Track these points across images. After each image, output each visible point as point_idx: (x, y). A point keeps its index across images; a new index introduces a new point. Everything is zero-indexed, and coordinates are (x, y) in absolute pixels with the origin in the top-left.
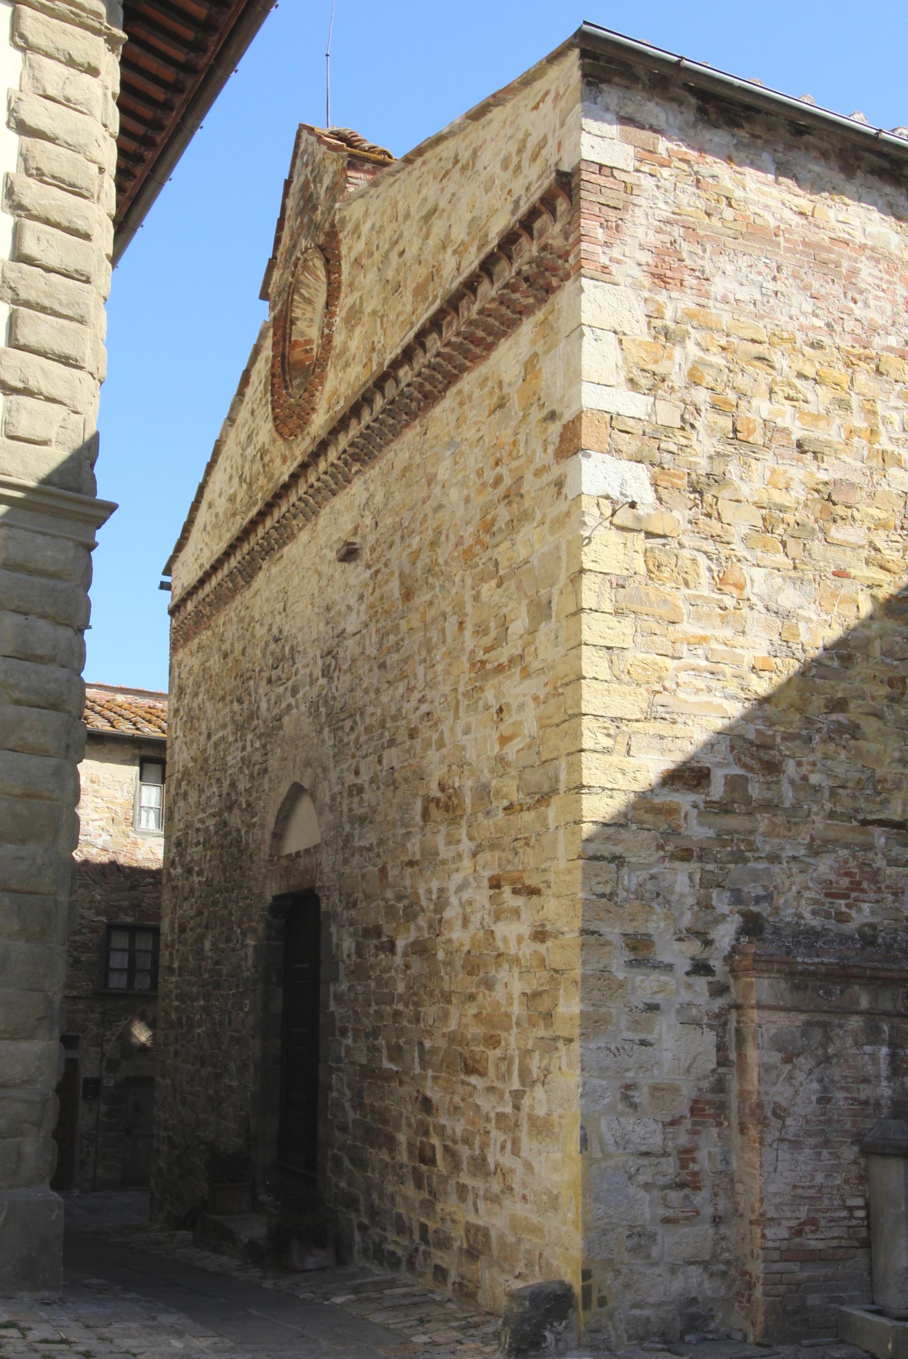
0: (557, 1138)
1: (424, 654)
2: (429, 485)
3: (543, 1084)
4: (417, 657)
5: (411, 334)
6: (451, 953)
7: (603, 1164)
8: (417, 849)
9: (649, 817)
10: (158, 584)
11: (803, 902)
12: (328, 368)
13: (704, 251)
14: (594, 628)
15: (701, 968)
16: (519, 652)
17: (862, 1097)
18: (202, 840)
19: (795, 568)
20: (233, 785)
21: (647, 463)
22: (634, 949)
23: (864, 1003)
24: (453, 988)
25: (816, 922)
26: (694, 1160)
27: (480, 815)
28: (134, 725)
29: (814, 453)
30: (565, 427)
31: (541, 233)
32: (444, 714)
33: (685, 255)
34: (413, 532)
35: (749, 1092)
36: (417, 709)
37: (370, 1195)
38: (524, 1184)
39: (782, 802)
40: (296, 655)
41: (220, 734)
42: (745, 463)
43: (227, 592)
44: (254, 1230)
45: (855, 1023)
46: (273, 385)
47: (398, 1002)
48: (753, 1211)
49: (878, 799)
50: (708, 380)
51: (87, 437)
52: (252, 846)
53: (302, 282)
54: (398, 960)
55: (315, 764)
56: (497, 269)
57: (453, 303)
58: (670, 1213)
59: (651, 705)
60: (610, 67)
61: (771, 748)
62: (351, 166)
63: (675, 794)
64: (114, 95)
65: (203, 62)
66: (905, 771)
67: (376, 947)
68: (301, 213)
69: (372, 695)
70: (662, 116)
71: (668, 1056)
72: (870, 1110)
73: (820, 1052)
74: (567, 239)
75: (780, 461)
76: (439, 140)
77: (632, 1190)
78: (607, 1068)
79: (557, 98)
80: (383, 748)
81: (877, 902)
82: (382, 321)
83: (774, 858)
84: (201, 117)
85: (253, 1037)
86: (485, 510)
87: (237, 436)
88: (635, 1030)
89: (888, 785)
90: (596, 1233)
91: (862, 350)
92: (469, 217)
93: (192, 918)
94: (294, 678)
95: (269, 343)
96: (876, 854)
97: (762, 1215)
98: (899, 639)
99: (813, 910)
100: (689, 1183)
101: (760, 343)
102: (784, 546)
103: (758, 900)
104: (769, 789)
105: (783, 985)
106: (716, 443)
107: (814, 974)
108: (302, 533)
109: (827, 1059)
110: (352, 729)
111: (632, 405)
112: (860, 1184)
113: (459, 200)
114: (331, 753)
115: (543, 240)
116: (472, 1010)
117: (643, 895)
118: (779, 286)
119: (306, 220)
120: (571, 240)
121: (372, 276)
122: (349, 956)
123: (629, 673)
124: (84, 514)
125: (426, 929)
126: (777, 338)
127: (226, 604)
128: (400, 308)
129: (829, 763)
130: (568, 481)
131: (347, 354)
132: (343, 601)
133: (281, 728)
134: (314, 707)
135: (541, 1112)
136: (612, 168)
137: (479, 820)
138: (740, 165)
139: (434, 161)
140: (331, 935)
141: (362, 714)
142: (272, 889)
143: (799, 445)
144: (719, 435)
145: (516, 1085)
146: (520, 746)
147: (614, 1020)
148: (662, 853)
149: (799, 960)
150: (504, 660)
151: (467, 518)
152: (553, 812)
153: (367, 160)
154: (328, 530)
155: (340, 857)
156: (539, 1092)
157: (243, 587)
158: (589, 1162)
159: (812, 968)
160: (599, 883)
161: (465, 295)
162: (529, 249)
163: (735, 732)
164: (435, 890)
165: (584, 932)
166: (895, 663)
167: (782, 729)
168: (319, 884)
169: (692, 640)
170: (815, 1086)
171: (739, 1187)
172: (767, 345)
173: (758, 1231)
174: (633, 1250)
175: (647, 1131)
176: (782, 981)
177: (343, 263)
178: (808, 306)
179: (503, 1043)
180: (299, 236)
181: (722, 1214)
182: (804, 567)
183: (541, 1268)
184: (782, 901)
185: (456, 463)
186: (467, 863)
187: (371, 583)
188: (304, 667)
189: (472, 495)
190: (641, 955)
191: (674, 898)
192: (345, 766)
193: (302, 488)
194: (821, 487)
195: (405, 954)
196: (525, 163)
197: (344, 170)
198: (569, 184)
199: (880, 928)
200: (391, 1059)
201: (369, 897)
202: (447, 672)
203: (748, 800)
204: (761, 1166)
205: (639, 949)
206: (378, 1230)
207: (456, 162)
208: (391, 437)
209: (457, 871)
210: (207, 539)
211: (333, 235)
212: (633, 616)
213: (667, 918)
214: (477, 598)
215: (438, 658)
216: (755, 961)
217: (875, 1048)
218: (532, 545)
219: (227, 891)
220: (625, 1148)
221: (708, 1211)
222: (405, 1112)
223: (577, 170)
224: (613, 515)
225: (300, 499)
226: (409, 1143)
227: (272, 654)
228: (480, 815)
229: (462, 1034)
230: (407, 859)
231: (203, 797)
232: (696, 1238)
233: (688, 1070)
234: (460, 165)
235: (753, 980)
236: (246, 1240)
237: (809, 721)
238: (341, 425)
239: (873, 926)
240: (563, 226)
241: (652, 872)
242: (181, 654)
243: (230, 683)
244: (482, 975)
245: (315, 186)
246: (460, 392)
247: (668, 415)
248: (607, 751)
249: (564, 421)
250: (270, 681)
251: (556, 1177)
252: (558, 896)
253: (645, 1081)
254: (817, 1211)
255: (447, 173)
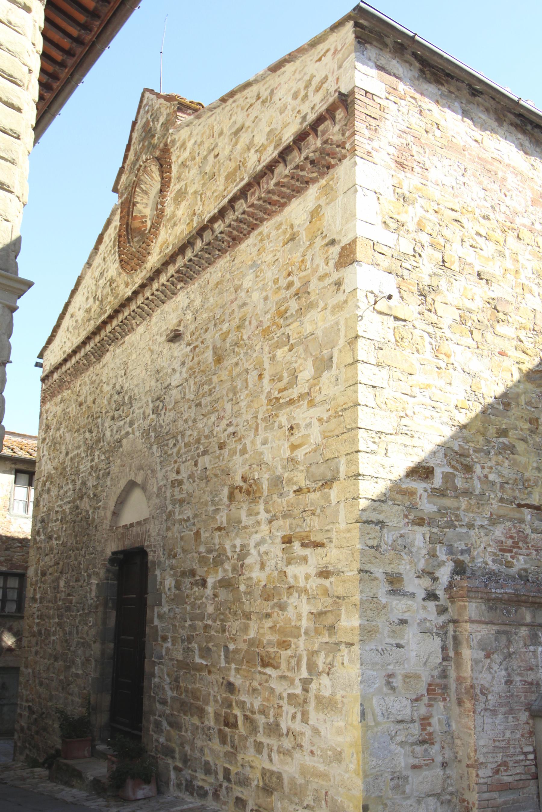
0: (341, 712)
1: (231, 395)
2: (236, 292)
3: (328, 674)
4: (225, 398)
5: (226, 200)
6: (251, 586)
7: (375, 730)
8: (224, 519)
9: (399, 497)
10: (34, 363)
11: (487, 554)
12: (161, 228)
13: (425, 152)
14: (364, 373)
15: (431, 596)
16: (307, 390)
17: (530, 680)
18: (60, 518)
19: (478, 348)
20: (84, 483)
21: (395, 274)
22: (391, 583)
23: (528, 619)
24: (251, 610)
25: (494, 567)
26: (430, 724)
27: (275, 497)
28: (12, 450)
29: (487, 280)
30: (343, 248)
31: (324, 133)
32: (246, 433)
33: (414, 153)
34: (224, 320)
35: (465, 678)
36: (226, 430)
37: (184, 748)
38: (311, 743)
39: (474, 491)
40: (134, 401)
41: (76, 452)
42: (450, 281)
43: (83, 366)
44: (100, 770)
45: (524, 631)
46: (119, 242)
47: (208, 619)
48: (469, 759)
49: (526, 491)
50: (428, 229)
51: (14, 238)
52: (97, 521)
53: (142, 180)
54: (209, 591)
55: (146, 468)
56: (289, 158)
57: (257, 179)
58: (416, 762)
59: (399, 425)
60: (373, 33)
61: (467, 456)
62: (179, 110)
63: (413, 483)
64: (40, 28)
65: (88, 38)
66: (540, 475)
67: (191, 583)
68: (143, 140)
69: (190, 423)
70: (401, 70)
71: (413, 654)
72: (534, 688)
73: (505, 651)
74: (343, 135)
75: (469, 283)
76: (248, 85)
77: (393, 747)
78: (377, 664)
79: (336, 52)
80: (198, 456)
81: (528, 555)
82: (201, 197)
83: (470, 526)
84: (84, 75)
85: (95, 642)
86: (280, 303)
87: (92, 274)
88: (393, 637)
89: (531, 483)
90: (371, 778)
91: (510, 224)
92: (268, 129)
93: (51, 567)
94: (131, 416)
95: (117, 217)
96: (526, 525)
97: (476, 761)
98: (534, 395)
99: (493, 559)
100: (426, 741)
101: (456, 211)
102: (472, 334)
103: (462, 552)
104: (467, 482)
105: (483, 607)
106: (433, 267)
107: (501, 599)
108: (139, 327)
109: (510, 655)
110: (175, 445)
111: (386, 237)
112: (530, 737)
113: (260, 120)
114: (158, 460)
115: (325, 138)
116: (268, 623)
117: (396, 548)
118: (465, 180)
119: (146, 144)
120: (347, 134)
121: (194, 171)
122: (169, 589)
123: (386, 403)
124: (9, 286)
125: (230, 571)
126: (465, 210)
127: (81, 374)
128: (215, 188)
129: (499, 468)
130: (346, 281)
131: (175, 218)
132: (169, 366)
133: (121, 446)
134: (146, 433)
135: (326, 693)
136: (373, 94)
137: (274, 499)
138: (443, 106)
139: (241, 100)
140: (156, 576)
141: (183, 436)
142: (111, 547)
143: (479, 275)
144: (435, 263)
145: (304, 674)
146: (308, 451)
147: (380, 631)
148: (407, 520)
149: (493, 590)
150: (295, 396)
151: (266, 310)
152: (334, 493)
153: (189, 107)
154: (159, 324)
155: (164, 526)
156: (325, 680)
157: (94, 362)
158: (366, 728)
159: (500, 596)
160: (370, 539)
161: (265, 174)
162: (314, 143)
163: (447, 445)
164: (238, 546)
165: (361, 571)
166: (533, 409)
167: (473, 445)
168: (147, 543)
169: (422, 386)
170: (503, 673)
171: (458, 742)
172: (459, 213)
173: (473, 772)
174: (396, 788)
175: (401, 706)
176: (483, 604)
177: (173, 166)
178: (482, 194)
179: (293, 646)
180: (141, 153)
181: (447, 760)
182: (482, 347)
183: (326, 802)
184: (475, 553)
185: (257, 277)
186: (264, 527)
187: (191, 355)
188: (139, 408)
189: (270, 295)
190: (396, 586)
191: (414, 549)
192: (169, 469)
193: (140, 300)
194: (490, 301)
195: (214, 588)
196: (311, 94)
197: (175, 112)
198: (346, 101)
199: (529, 572)
200: (202, 657)
201: (186, 551)
202: (249, 406)
203: (455, 488)
204: (475, 728)
205: (394, 581)
206: (190, 771)
207: (258, 98)
208: (207, 265)
209: (256, 532)
210: (69, 336)
211: (166, 150)
212: (388, 368)
213: (411, 563)
214: (273, 358)
215: (242, 398)
216: (468, 591)
217: (535, 647)
218: (316, 324)
219: (78, 550)
220: (388, 718)
221: (439, 759)
222: (212, 692)
223: (352, 92)
224: (375, 304)
225: (138, 307)
226: (215, 713)
227: (115, 401)
228: (275, 497)
229: (260, 640)
230: (216, 526)
231: (62, 491)
232: (431, 778)
233: (425, 664)
234: (261, 100)
235: (466, 603)
236: (91, 778)
237: (488, 441)
238: (171, 259)
239: (526, 570)
240: (341, 127)
241: (402, 532)
242: (48, 405)
243: (83, 421)
244: (276, 600)
245: (154, 123)
246: (261, 233)
247: (406, 247)
248: (374, 452)
249: (342, 244)
250: (113, 418)
251: (340, 739)
252: (339, 547)
253: (400, 672)
254: (507, 756)
255: (251, 105)
